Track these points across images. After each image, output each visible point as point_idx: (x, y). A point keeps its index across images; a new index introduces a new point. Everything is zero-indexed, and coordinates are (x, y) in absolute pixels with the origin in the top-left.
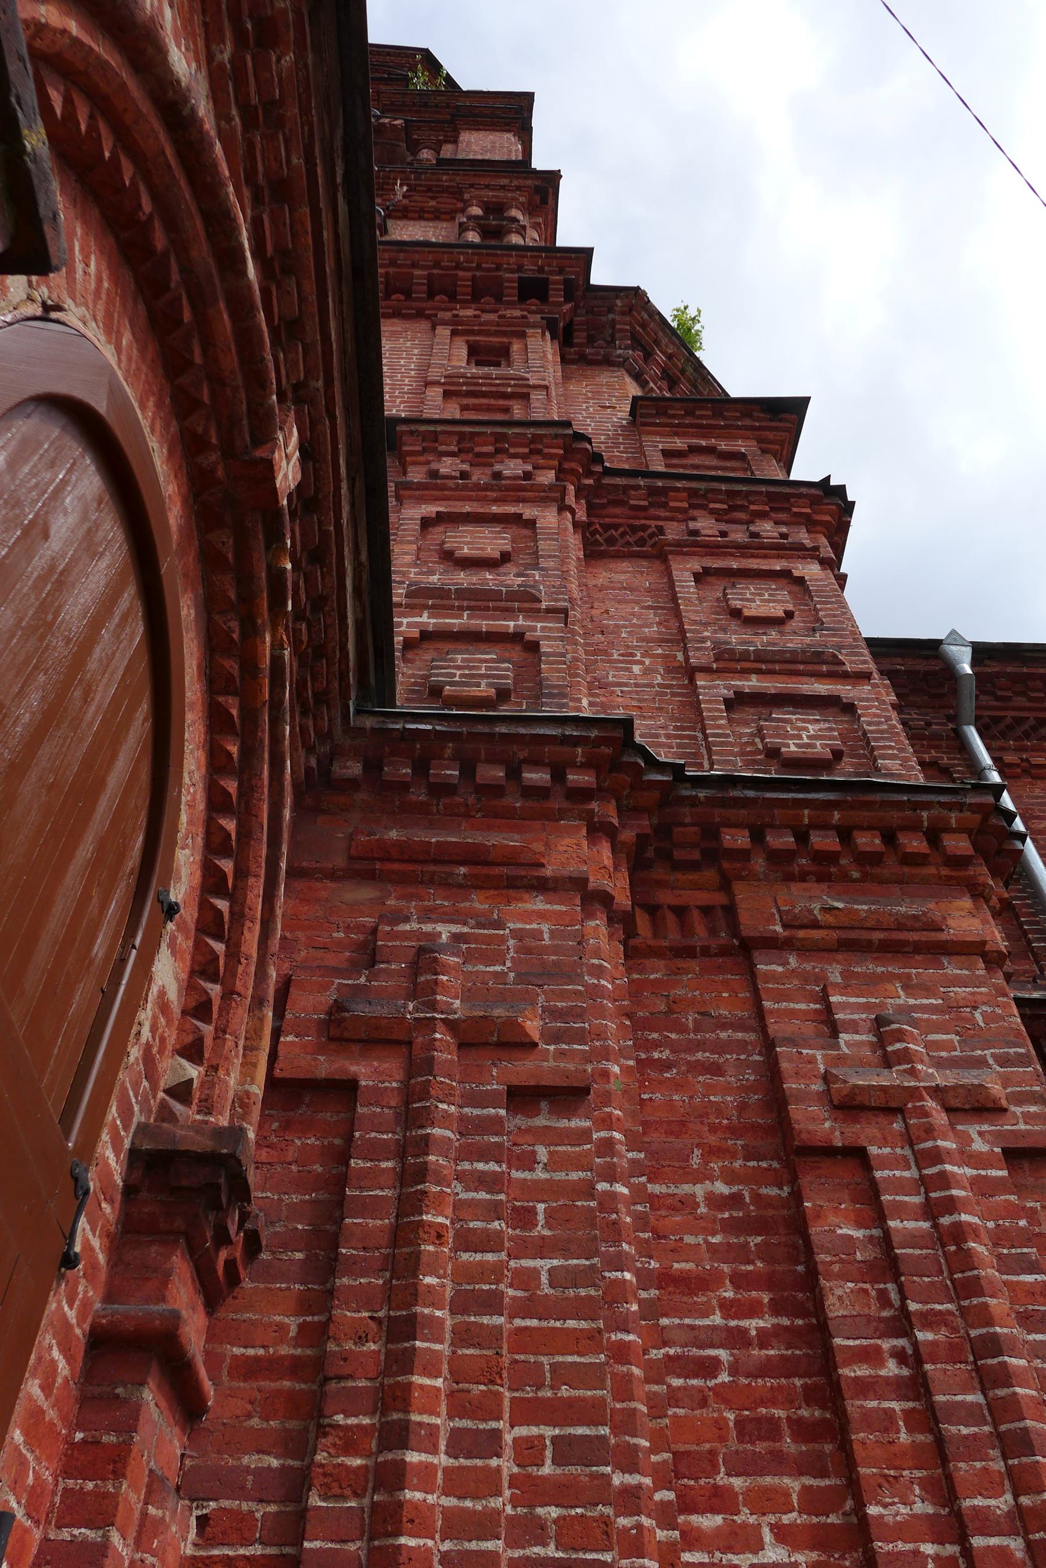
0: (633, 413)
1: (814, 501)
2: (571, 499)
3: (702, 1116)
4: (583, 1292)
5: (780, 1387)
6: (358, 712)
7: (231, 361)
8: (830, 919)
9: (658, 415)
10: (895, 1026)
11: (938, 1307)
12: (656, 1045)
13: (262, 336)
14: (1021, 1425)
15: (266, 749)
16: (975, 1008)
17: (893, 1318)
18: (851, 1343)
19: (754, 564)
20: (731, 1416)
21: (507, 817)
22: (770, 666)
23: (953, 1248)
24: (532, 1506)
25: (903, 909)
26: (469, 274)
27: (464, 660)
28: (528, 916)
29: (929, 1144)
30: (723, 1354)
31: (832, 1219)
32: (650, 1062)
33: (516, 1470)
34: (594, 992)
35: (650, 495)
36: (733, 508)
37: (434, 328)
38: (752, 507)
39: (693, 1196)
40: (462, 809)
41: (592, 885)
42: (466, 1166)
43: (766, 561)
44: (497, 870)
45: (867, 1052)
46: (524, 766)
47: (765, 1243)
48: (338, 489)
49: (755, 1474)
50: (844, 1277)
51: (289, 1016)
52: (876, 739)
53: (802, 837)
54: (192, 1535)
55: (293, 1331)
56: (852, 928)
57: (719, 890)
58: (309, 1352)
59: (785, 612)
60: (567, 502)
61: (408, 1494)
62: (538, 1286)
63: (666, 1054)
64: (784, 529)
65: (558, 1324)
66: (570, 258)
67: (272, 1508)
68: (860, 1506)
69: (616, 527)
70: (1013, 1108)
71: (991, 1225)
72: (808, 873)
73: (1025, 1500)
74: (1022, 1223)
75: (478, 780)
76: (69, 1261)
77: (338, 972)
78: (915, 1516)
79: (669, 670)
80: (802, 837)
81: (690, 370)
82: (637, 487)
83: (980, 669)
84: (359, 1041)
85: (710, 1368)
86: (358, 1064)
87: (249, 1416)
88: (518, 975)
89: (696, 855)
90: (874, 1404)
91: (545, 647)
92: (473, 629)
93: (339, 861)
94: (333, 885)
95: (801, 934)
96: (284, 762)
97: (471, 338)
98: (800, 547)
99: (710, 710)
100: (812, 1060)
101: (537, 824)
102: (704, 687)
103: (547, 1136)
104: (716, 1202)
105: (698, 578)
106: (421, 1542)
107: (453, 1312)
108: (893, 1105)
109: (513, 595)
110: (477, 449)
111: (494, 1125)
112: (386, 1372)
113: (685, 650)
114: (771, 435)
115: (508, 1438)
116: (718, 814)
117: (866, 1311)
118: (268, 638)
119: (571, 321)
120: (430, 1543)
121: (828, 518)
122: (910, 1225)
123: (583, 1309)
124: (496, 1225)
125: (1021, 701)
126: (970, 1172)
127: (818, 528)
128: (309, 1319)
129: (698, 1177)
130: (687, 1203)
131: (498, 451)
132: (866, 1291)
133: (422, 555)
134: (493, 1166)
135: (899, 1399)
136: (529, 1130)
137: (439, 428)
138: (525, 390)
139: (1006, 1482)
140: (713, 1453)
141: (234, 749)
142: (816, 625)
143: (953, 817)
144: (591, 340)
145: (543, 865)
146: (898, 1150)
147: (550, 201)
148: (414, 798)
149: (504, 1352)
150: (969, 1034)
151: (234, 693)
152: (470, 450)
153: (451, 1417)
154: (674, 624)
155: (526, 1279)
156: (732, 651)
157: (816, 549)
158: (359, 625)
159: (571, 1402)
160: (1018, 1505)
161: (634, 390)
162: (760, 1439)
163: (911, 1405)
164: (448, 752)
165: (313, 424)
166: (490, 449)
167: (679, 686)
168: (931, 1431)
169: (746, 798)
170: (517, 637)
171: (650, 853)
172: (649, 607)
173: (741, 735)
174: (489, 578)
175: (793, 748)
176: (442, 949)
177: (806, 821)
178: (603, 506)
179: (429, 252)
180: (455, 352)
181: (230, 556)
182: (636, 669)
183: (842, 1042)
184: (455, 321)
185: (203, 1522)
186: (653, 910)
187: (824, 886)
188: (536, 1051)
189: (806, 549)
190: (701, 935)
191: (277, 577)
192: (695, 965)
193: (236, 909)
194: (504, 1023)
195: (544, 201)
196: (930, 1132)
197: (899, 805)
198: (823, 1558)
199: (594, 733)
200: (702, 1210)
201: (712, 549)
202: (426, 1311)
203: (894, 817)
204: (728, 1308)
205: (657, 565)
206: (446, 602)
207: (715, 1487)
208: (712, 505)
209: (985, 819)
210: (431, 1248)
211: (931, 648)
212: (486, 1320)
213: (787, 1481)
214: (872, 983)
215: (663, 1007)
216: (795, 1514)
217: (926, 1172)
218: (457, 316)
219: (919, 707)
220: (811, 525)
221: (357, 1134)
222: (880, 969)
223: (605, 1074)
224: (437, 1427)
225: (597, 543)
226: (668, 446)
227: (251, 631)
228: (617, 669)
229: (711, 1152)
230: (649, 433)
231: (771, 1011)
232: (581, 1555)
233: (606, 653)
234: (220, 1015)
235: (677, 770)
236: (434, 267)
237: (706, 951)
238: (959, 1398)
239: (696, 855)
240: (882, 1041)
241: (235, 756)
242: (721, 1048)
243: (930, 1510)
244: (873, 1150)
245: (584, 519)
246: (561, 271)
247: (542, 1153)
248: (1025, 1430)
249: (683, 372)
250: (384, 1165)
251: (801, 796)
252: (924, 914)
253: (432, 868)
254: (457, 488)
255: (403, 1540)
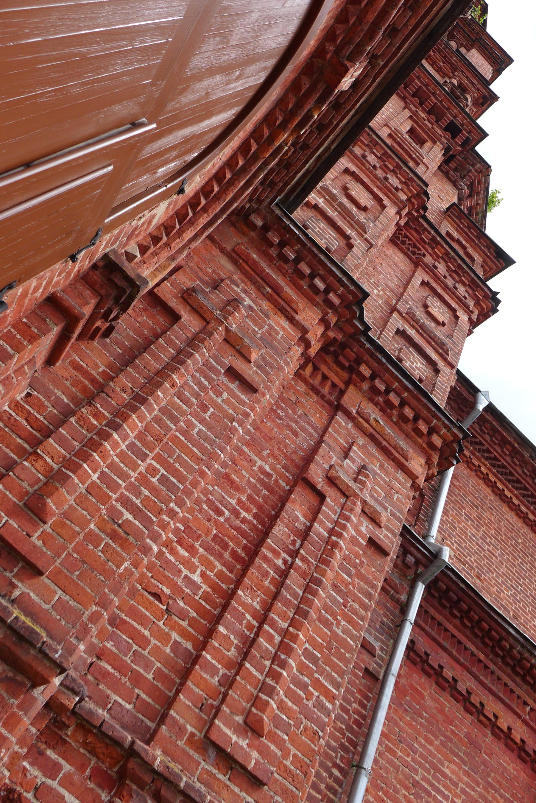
0: (448, 209)
1: (486, 297)
2: (404, 213)
3: (279, 443)
4: (206, 445)
5: (237, 538)
6: (277, 204)
7: (371, 17)
8: (374, 424)
9: (457, 217)
10: (367, 472)
11: (310, 559)
12: (282, 409)
13: (388, 19)
14: (308, 609)
15: (250, 175)
16: (397, 493)
17: (292, 550)
18: (273, 544)
19: (446, 297)
20: (215, 531)
21: (299, 288)
22: (423, 333)
23: (330, 547)
24: (141, 485)
25: (401, 443)
26: (436, 101)
27: (323, 227)
28: (279, 324)
29: (348, 514)
30: (227, 513)
31: (297, 507)
32: (275, 412)
33: (144, 471)
34: (280, 368)
35: (431, 240)
36: (456, 272)
37: (404, 108)
38: (463, 278)
39: (256, 462)
40: (284, 271)
41: (308, 336)
42: (198, 375)
43: (451, 300)
44: (280, 301)
45: (351, 472)
46: (318, 277)
47: (268, 496)
48: (351, 110)
49: (209, 553)
50: (287, 526)
51: (173, 277)
52: (438, 388)
53: (388, 391)
54: (23, 395)
55: (101, 370)
56: (379, 434)
57: (344, 383)
58: (101, 380)
59: (443, 322)
60: (402, 213)
61: (106, 444)
62: (193, 430)
63: (283, 414)
64: (467, 296)
65: (190, 446)
66: (477, 131)
67: (55, 411)
68: (237, 587)
69: (410, 240)
70: (383, 529)
71: (347, 553)
72: (379, 404)
73: (291, 629)
74: (358, 561)
75: (299, 266)
76: (73, 258)
77: (201, 280)
78: (252, 605)
79: (386, 302)
80: (388, 391)
81: (480, 216)
82: (429, 233)
83: (485, 414)
84: (192, 307)
85: (220, 513)
86: (185, 313)
87: (67, 380)
88: (261, 337)
89: (347, 364)
90: (265, 566)
91: (355, 249)
92: (335, 220)
93: (229, 248)
94: (220, 253)
95: (361, 420)
96: (251, 187)
97: (415, 125)
98: (467, 307)
99: (390, 327)
100: (331, 458)
101: (306, 300)
102: (394, 318)
103: (230, 391)
104: (262, 470)
105: (423, 283)
106: (100, 461)
107: (159, 411)
108: (347, 493)
109: (358, 223)
110: (387, 163)
111: (217, 373)
112: (125, 407)
113: (398, 301)
114: (490, 263)
115: (148, 461)
116: (366, 357)
117: (285, 541)
118: (286, 136)
119: (455, 155)
120: (102, 464)
121: (485, 307)
122: (321, 530)
123: (201, 448)
124: (194, 400)
125: (488, 437)
126: (353, 533)
127: (479, 307)
128: (109, 371)
129: (262, 458)
130: (252, 462)
131: (393, 171)
132: (290, 536)
133: (336, 180)
134: (206, 383)
135: (275, 572)
136: (226, 385)
137: (380, 142)
138: (419, 161)
139: (289, 621)
140: (200, 536)
141: (241, 163)
142: (450, 336)
143: (443, 431)
144: (455, 170)
145: (297, 314)
146: (336, 507)
147: (485, 107)
148: (271, 252)
149: (168, 436)
150: (388, 496)
151: (258, 144)
152: (383, 161)
153: (135, 438)
154: (401, 290)
155: (191, 425)
156: (414, 315)
157: (472, 312)
158: (308, 172)
159: (176, 470)
160: (287, 629)
161: (455, 200)
162: (219, 545)
163: (277, 577)
164: (297, 247)
165: (366, 76)
166: (391, 168)
167: (385, 311)
168: (277, 589)
169: (381, 361)
170: (347, 238)
171: (332, 349)
172: (397, 277)
173: (393, 345)
174: (354, 210)
175: (407, 364)
176: (243, 305)
177: (394, 387)
178: (411, 228)
179: (428, 78)
180: (405, 124)
181: (303, 91)
182: (376, 291)
183: (345, 462)
184: (415, 113)
185: (29, 395)
186: (316, 369)
187: (381, 413)
188: (35, 581)
189: (468, 309)
190: (326, 390)
191: (308, 116)
192: (315, 398)
193: (193, 220)
194: (246, 346)
195: (483, 104)
196: (352, 510)
197: (429, 410)
198: (211, 593)
199: (352, 288)
200: (255, 468)
201: (436, 278)
202: (152, 401)
203: (424, 412)
204: (239, 501)
205: (412, 266)
206: (332, 202)
207: (193, 545)
208: (449, 264)
209: (453, 442)
210: (168, 386)
211: (474, 390)
212: (169, 422)
213: (217, 564)
214: (370, 455)
215: (294, 400)
216: (212, 574)
217: (340, 520)
218: (417, 112)
219: (451, 408)
220: (477, 303)
221: (168, 333)
222: (376, 454)
223: (264, 395)
224: (129, 436)
225: (398, 238)
226: (451, 232)
227: (283, 126)
228: (369, 285)
229: (273, 455)
230: (448, 221)
231: (330, 433)
232: (146, 511)
233: (369, 276)
234: (159, 248)
235: (367, 328)
236: (425, 86)
237: (323, 397)
238: (295, 587)
239: (347, 364)
240: (359, 473)
241: (239, 166)
242: (303, 429)
243: (258, 607)
244: (328, 500)
245: (402, 225)
246: (469, 133)
247: (225, 395)
248: (309, 612)
249: (477, 214)
250: (170, 350)
251: (400, 377)
252: (407, 451)
253: (259, 279)
254: (368, 169)
255: (95, 454)
